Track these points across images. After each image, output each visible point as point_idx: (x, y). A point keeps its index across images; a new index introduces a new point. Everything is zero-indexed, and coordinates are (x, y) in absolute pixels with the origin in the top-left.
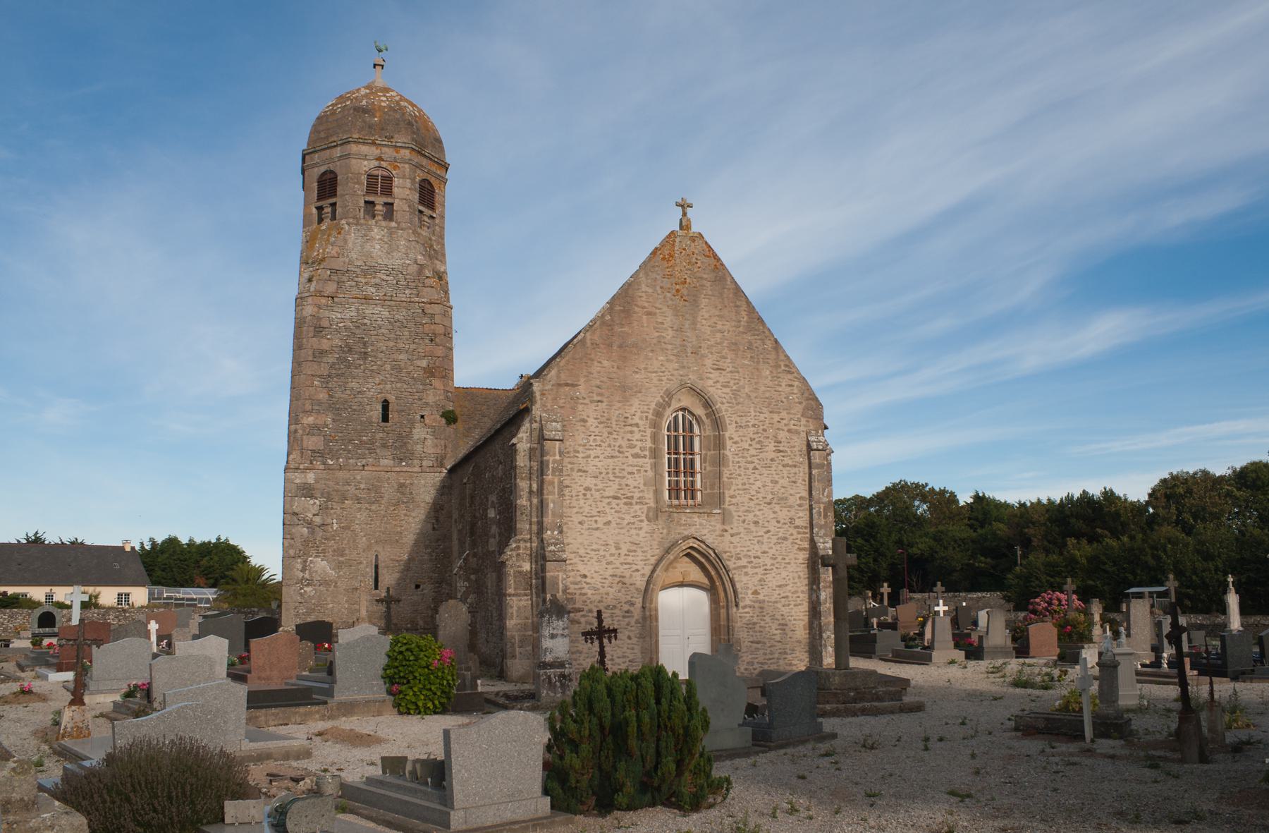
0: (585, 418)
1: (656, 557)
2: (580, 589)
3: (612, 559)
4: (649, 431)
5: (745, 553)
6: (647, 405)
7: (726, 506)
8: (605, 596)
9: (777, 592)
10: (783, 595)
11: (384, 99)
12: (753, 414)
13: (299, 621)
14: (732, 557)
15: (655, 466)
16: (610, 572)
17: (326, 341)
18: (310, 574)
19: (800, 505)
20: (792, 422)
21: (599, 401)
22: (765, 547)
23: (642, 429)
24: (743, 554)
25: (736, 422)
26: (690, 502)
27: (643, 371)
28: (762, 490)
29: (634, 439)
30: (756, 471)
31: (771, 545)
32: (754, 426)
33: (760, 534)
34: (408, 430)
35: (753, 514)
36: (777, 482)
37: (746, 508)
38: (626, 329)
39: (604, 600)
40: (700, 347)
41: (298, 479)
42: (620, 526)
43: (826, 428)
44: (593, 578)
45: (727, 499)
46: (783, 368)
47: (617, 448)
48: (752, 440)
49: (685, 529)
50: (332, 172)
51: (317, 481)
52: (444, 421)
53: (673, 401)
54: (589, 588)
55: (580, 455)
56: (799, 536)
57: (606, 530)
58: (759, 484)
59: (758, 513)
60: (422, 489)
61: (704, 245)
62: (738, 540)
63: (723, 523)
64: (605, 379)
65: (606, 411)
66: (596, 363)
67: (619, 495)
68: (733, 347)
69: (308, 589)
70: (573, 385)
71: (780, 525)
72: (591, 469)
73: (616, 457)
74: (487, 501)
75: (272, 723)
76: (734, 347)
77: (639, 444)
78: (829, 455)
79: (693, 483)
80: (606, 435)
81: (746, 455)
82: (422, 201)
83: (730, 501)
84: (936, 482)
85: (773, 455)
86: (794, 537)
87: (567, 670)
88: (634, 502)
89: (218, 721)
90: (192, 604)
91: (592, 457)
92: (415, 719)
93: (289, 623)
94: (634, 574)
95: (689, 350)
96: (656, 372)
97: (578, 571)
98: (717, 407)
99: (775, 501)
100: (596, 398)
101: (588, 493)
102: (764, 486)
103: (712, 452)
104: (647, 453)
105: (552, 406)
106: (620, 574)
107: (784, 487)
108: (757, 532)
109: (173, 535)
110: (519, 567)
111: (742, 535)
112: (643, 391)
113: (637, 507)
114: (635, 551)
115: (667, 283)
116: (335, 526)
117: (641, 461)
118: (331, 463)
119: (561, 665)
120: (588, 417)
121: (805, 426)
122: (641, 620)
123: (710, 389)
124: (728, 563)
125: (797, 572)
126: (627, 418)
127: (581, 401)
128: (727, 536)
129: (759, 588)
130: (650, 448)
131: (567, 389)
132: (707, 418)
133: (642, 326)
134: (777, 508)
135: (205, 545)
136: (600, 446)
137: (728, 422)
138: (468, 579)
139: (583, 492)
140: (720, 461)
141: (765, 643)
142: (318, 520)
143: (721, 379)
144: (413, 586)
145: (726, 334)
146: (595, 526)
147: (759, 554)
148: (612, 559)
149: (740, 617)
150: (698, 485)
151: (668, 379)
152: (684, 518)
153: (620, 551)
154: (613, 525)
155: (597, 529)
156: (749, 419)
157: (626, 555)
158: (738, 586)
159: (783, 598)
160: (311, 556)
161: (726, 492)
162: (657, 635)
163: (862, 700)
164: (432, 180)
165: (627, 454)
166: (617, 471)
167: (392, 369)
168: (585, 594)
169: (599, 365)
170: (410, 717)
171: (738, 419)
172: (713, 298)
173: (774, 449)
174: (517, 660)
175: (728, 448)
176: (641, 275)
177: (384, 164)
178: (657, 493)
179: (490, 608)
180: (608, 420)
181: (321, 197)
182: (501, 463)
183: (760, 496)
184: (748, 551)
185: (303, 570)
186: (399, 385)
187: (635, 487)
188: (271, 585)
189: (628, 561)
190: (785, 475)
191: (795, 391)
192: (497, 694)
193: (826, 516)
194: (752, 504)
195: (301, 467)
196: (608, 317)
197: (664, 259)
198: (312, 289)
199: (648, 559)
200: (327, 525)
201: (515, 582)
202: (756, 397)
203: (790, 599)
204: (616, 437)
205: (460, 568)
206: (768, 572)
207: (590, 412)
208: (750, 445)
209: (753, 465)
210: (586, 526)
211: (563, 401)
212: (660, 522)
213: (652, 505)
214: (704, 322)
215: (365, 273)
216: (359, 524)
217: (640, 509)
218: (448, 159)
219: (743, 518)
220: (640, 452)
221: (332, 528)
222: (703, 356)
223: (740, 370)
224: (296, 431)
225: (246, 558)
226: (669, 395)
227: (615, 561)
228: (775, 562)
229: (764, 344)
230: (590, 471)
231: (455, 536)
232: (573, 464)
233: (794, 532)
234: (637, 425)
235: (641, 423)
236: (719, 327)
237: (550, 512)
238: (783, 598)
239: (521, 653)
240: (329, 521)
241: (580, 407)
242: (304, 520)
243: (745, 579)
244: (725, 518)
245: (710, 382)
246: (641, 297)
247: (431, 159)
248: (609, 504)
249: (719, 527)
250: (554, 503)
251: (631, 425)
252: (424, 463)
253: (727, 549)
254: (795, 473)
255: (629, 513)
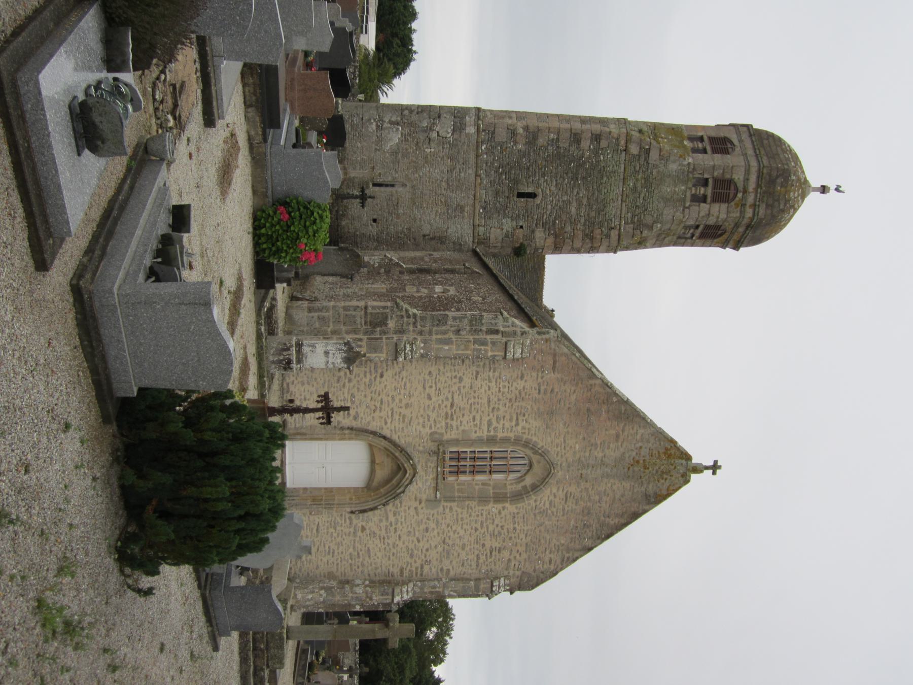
0: (525, 378)
1: (397, 441)
2: (370, 371)
3: (397, 400)
4: (512, 435)
5: (400, 520)
6: (535, 434)
7: (443, 503)
8: (363, 394)
9: (363, 549)
10: (361, 553)
11: (796, 195)
12: (526, 528)
13: (346, 117)
14: (397, 508)
15: (480, 441)
16: (385, 399)
17: (588, 144)
18: (387, 128)
19: (442, 570)
20: (517, 564)
21: (539, 390)
22: (404, 538)
23: (514, 429)
24: (399, 518)
25: (518, 513)
26: (447, 470)
27: (566, 430)
28: (456, 535)
29: (505, 422)
30: (473, 531)
31: (406, 543)
32: (515, 529)
33: (417, 533)
34: (510, 216)
35: (435, 527)
36: (463, 549)
37: (440, 521)
38: (604, 415)
39: (360, 393)
40: (587, 481)
41: (470, 120)
42: (426, 409)
43: (511, 593)
44: (380, 383)
45: (449, 504)
46: (567, 555)
47: (496, 406)
48: (502, 527)
49: (422, 466)
50: (733, 150)
51: (467, 135)
52: (517, 245)
53: (538, 457)
54: (370, 380)
55: (491, 374)
56: (414, 569)
57: (423, 395)
58: (462, 532)
59: (436, 532)
60: (459, 227)
61: (678, 486)
62: (412, 514)
63: (427, 500)
64: (559, 396)
65: (530, 397)
66: (573, 389)
67: (455, 408)
68: (586, 511)
69: (374, 126)
70: (554, 368)
71: (424, 551)
72: (478, 383)
73: (489, 406)
74: (449, 285)
75: (247, 90)
76: (587, 512)
77: (501, 426)
78: (487, 596)
79: (464, 472)
80: (509, 396)
81: (489, 521)
82: (707, 227)
83: (447, 507)
84: (453, 646)
85: (488, 546)
86: (413, 564)
87: (294, 365)
88: (448, 421)
89: (233, 28)
90: (362, 28)
91: (490, 384)
92: (248, 225)
93: (342, 106)
94: (383, 420)
95: (584, 472)
96: (565, 441)
97: (387, 370)
98: (533, 496)
99: (446, 547)
100: (542, 388)
101: (457, 380)
102: (460, 537)
103: (491, 491)
104: (492, 433)
105: (536, 348)
106: (383, 407)
107: (459, 555)
108: (419, 531)
109: (419, 16)
110: (391, 317)
111: (416, 517)
112: (548, 430)
113: (443, 424)
114: (404, 421)
115: (644, 452)
116: (428, 151)
117: (485, 428)
118: (483, 148)
119: (299, 361)
120: (526, 381)
121: (514, 574)
122: (341, 425)
123: (549, 489)
124: (391, 505)
125: (381, 566)
126: (524, 415)
127: (540, 374)
128: (416, 504)
129: (368, 532)
130: (497, 436)
131: (551, 362)
132: (522, 487)
133: (606, 430)
134: (440, 549)
135: (410, 42)
136: (499, 391)
137: (519, 505)
138: (380, 266)
139: (458, 376)
140: (483, 499)
141: (317, 536)
142: (434, 135)
143: (557, 500)
144: (375, 217)
145: (598, 504)
146: (427, 386)
147: (399, 532)
148: (397, 400)
149: (341, 515)
150: (462, 478)
151: (558, 452)
152: (433, 465)
153: (404, 408)
154: (427, 402)
155: (424, 388)
156: (521, 524)
157: (400, 413)
158: (370, 513)
159: (358, 554)
160: (402, 129)
161: (456, 504)
162: (327, 439)
163: (255, 656)
164: (725, 236)
165: (491, 415)
166: (476, 406)
167: (563, 201)
168: (365, 376)
169: (572, 391)
170: (251, 221)
171: (521, 515)
172: (630, 493)
173: (494, 547)
174: (306, 314)
175: (495, 506)
176: (652, 429)
177: (740, 195)
178: (456, 442)
179: (355, 286)
180: (523, 399)
181: (712, 140)
182: (484, 299)
183: (451, 534)
184: (402, 523)
185: (391, 122)
186: (549, 207)
187: (461, 422)
188: (377, 92)
189: (395, 415)
190: (470, 557)
191: (545, 566)
192: (274, 299)
193: (431, 593)
194: (444, 526)
195: (480, 122)
196: (615, 399)
197: (666, 449)
198: (633, 133)
199: (396, 433)
200: (429, 143)
201: (378, 313)
202: (540, 531)
203: (357, 560)
204: (507, 406)
205: (391, 260)
206: (382, 540)
207: (529, 383)
208: (497, 526)
209: (479, 527)
210: (427, 377)
211: (540, 359)
212: (430, 444)
213: (445, 437)
214: (609, 485)
215: (647, 179)
216: (429, 171)
217: (442, 427)
218: (743, 250)
219: (432, 519)
220: (493, 426)
221: (427, 148)
222: (578, 483)
223: (565, 517)
224: (511, 118)
225: (400, 74)
226: (543, 454)
227: (395, 403)
228: (391, 546)
229: (589, 539)
230: (476, 382)
231: (418, 254)
232: (484, 367)
233: (418, 564)
234: (517, 424)
235: (519, 428)
236: (604, 498)
237: (441, 346)
238: (358, 554)
239: (313, 317)
240: (433, 145)
241: (534, 374)
242: (433, 124)
243: (376, 519)
244: (433, 502)
245: (554, 490)
246: (633, 429)
247: (743, 235)
248: (447, 399)
249: (424, 497)
250: (448, 350)
251: (517, 419)
252: (481, 229)
253: (404, 504)
254: (471, 566)
255: (438, 416)
